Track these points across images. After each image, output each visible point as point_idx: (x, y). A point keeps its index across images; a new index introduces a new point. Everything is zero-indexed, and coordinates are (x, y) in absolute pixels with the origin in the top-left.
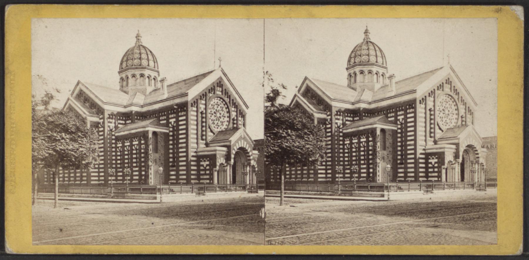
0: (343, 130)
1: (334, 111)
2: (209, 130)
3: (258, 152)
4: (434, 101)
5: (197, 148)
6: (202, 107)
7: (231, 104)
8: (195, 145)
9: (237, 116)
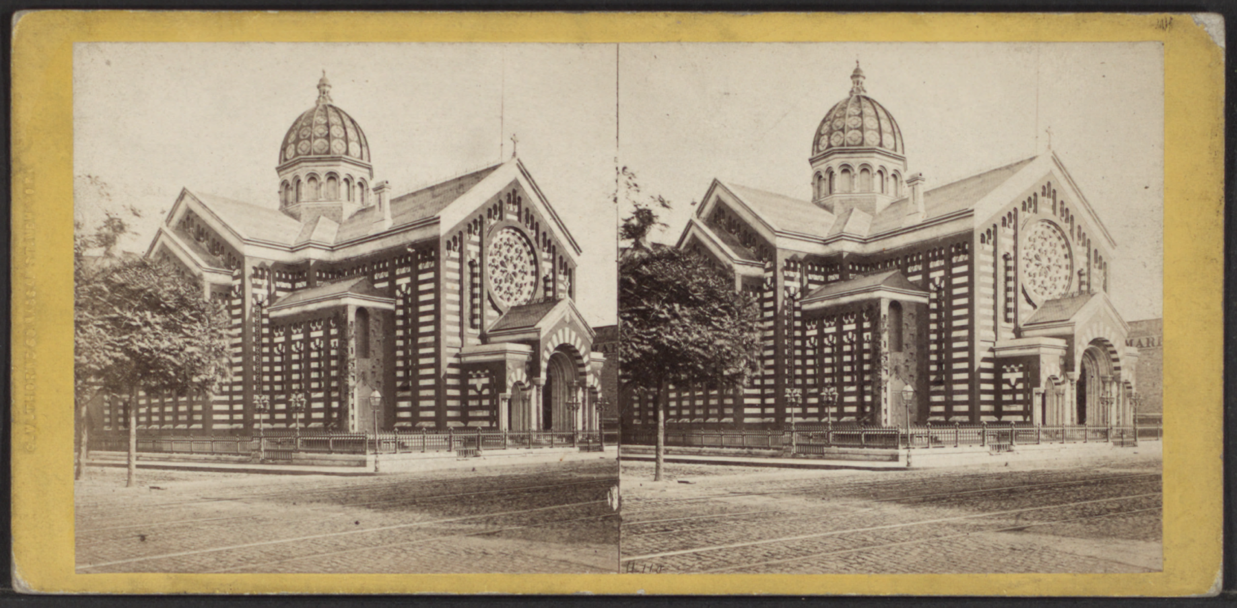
0: (801, 304)
1: (781, 259)
2: (489, 304)
3: (605, 356)
4: (1015, 237)
5: (460, 345)
6: (472, 250)
7: (541, 244)
8: (457, 340)
9: (553, 271)
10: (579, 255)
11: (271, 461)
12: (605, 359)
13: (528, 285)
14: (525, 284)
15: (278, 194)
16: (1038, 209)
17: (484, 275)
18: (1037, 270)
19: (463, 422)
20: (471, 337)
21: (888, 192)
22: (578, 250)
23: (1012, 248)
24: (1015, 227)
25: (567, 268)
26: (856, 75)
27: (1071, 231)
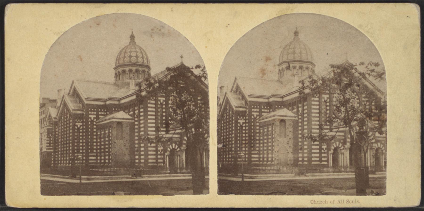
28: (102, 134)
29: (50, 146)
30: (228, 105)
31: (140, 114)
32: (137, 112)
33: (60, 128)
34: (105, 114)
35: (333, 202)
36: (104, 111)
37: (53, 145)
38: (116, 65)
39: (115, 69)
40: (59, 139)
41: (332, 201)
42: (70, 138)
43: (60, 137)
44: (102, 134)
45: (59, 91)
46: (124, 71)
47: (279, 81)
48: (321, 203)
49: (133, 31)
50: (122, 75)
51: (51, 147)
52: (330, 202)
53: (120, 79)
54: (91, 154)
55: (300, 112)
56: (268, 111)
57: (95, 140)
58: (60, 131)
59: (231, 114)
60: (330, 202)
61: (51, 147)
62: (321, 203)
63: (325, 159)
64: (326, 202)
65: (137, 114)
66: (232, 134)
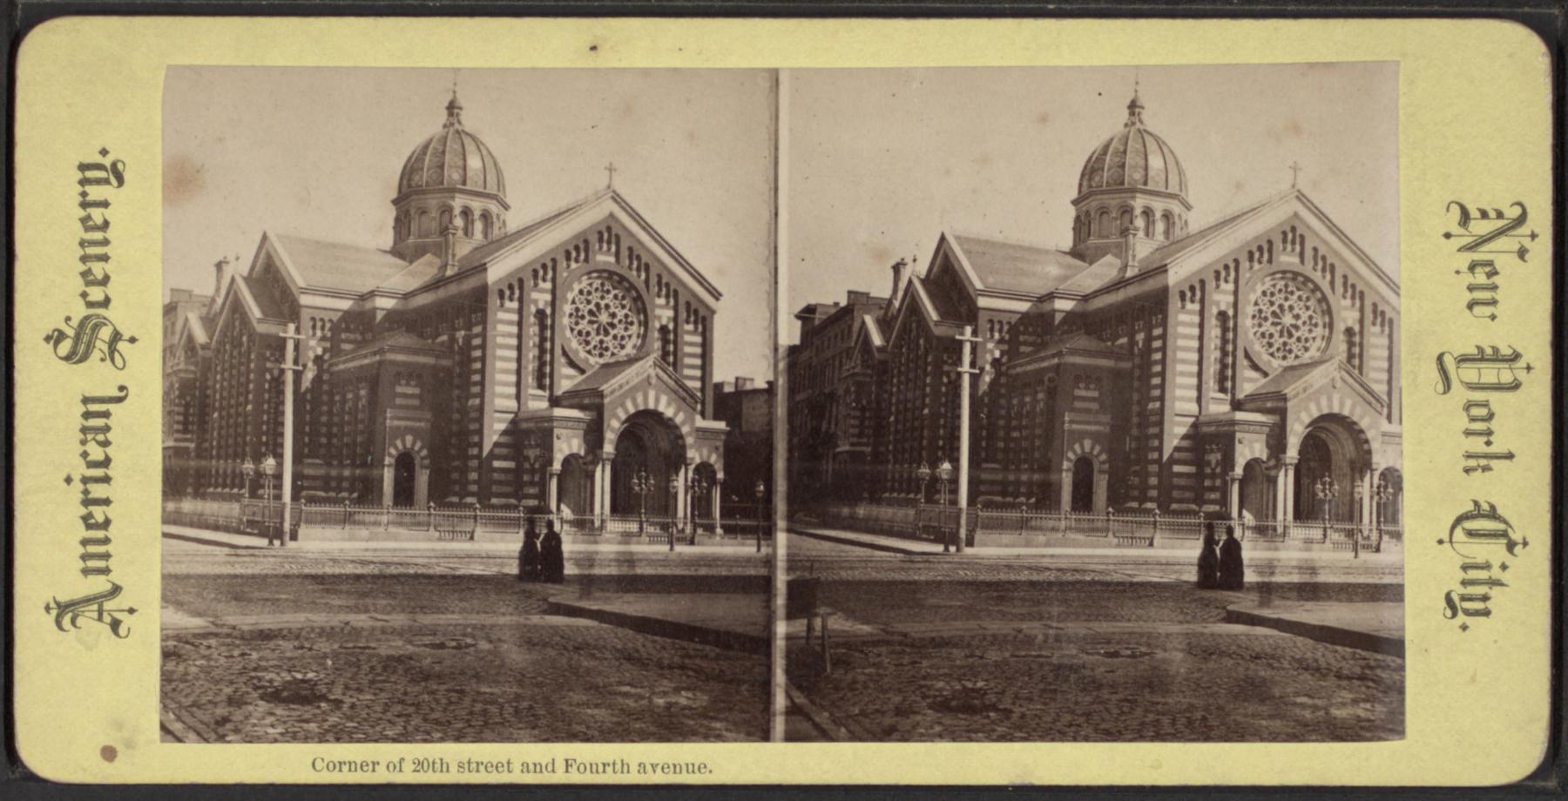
0: (1008, 368)
2: (563, 360)
3: (727, 425)
6: (541, 298)
7: (1339, 289)
8: (513, 404)
9: (675, 319)
10: (717, 299)
11: (719, 563)
12: (728, 429)
13: (634, 338)
14: (1314, 339)
15: (607, 213)
16: (1274, 258)
17: (1239, 329)
18: (1275, 330)
19: (516, 499)
20: (533, 400)
21: (1154, 235)
22: (717, 295)
23: (1231, 305)
24: (1236, 281)
25: (1384, 319)
26: (452, 108)
27: (1332, 283)
28: (1038, 401)
29: (185, 431)
30: (237, 316)
31: (1150, 345)
32: (1140, 337)
33: (218, 377)
34: (1039, 341)
35: (398, 769)
36: (1034, 333)
37: (871, 432)
38: (1080, 191)
39: (1075, 202)
40: (891, 414)
41: (396, 760)
42: (246, 406)
43: (893, 409)
44: (1038, 401)
45: (219, 266)
46: (1104, 211)
47: (1076, 253)
48: (604, 771)
49: (457, 89)
50: (1097, 221)
51: (865, 440)
52: (388, 767)
53: (409, 235)
54: (309, 461)
55: (1140, 344)
56: (359, 337)
57: (1001, 423)
58: (218, 386)
59: (922, 347)
60: (388, 767)
61: (189, 436)
62: (478, 771)
63: (532, 491)
64: (444, 766)
65: (460, 343)
66: (247, 402)
